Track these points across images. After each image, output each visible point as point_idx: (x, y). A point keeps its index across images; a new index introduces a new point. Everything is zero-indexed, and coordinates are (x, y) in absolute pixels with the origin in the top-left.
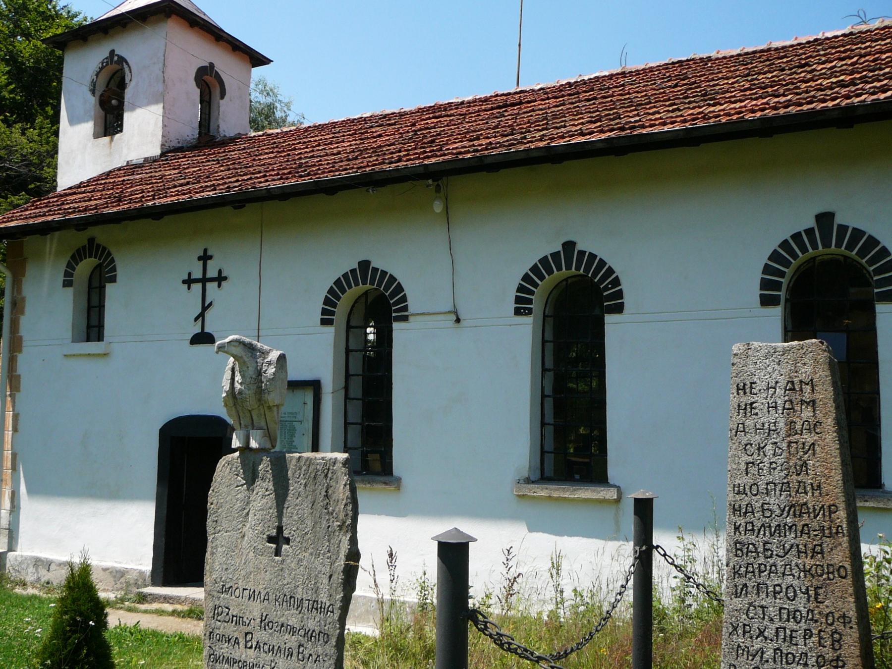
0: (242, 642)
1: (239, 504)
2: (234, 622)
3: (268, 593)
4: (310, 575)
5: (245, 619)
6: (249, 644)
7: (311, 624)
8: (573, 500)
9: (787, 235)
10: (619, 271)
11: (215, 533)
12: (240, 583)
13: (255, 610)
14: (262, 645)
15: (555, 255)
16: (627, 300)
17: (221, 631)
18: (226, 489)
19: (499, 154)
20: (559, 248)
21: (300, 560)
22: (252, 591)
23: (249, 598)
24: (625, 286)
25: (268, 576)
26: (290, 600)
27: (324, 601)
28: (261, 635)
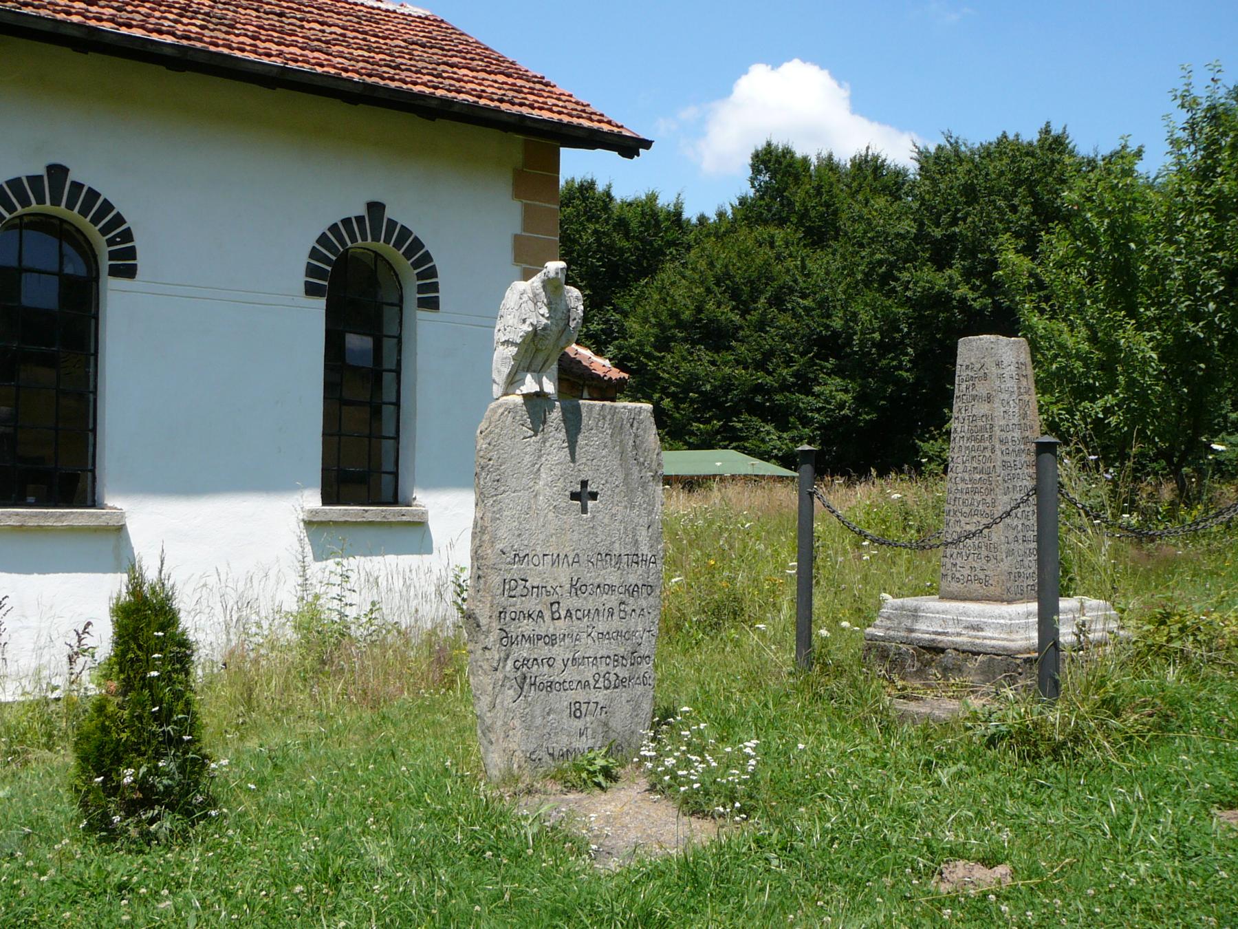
0: (547, 615)
1: (527, 459)
2: (535, 595)
3: (577, 555)
4: (626, 528)
5: (549, 588)
6: (557, 615)
7: (632, 579)
8: (72, 529)
9: (337, 219)
10: (131, 221)
11: (496, 495)
12: (539, 549)
13: (563, 575)
14: (573, 613)
15: (35, 180)
16: (141, 261)
17: (518, 608)
18: (509, 442)
19: (10, 11)
20: (40, 170)
21: (613, 515)
22: (555, 555)
23: (553, 564)
24: (139, 242)
25: (576, 536)
26: (607, 556)
27: (645, 553)
28: (569, 602)
